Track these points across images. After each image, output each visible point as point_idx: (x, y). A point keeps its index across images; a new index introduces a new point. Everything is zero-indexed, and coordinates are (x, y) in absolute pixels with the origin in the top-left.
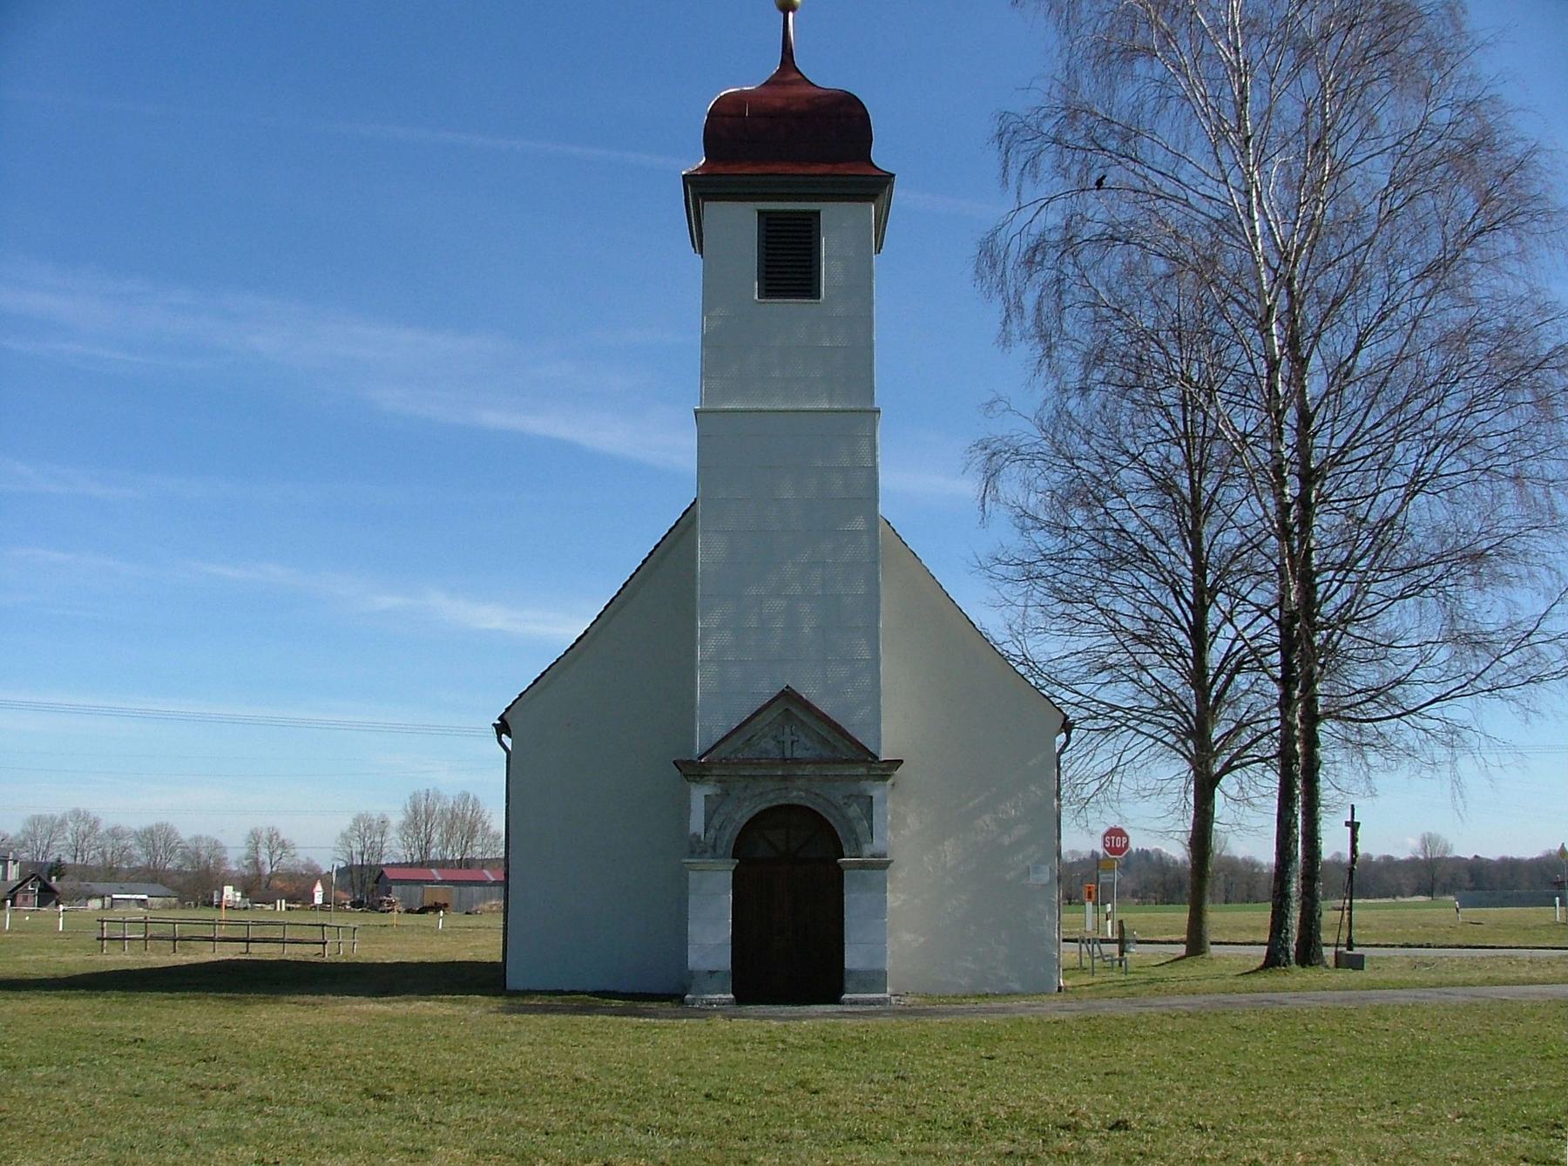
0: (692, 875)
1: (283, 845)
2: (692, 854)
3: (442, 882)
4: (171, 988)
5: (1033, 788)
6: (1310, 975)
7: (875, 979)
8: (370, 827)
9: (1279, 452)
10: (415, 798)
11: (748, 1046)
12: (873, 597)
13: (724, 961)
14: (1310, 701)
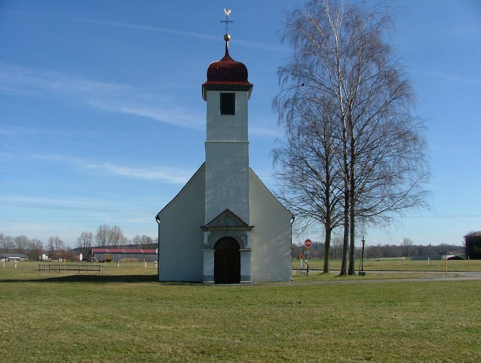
0: (205, 254)
1: (60, 242)
2: (205, 248)
3: (109, 253)
4: (68, 281)
5: (285, 232)
6: (351, 277)
7: (248, 278)
8: (87, 236)
9: (345, 151)
10: (100, 227)
11: (223, 291)
12: (248, 187)
13: (212, 273)
14: (352, 211)
